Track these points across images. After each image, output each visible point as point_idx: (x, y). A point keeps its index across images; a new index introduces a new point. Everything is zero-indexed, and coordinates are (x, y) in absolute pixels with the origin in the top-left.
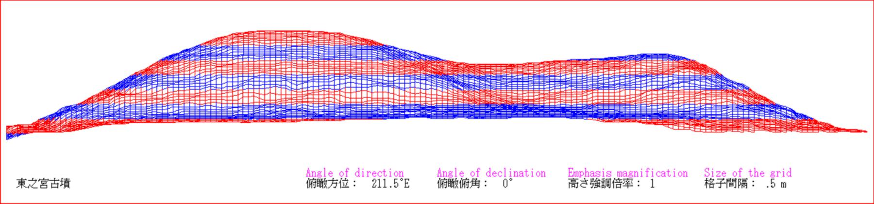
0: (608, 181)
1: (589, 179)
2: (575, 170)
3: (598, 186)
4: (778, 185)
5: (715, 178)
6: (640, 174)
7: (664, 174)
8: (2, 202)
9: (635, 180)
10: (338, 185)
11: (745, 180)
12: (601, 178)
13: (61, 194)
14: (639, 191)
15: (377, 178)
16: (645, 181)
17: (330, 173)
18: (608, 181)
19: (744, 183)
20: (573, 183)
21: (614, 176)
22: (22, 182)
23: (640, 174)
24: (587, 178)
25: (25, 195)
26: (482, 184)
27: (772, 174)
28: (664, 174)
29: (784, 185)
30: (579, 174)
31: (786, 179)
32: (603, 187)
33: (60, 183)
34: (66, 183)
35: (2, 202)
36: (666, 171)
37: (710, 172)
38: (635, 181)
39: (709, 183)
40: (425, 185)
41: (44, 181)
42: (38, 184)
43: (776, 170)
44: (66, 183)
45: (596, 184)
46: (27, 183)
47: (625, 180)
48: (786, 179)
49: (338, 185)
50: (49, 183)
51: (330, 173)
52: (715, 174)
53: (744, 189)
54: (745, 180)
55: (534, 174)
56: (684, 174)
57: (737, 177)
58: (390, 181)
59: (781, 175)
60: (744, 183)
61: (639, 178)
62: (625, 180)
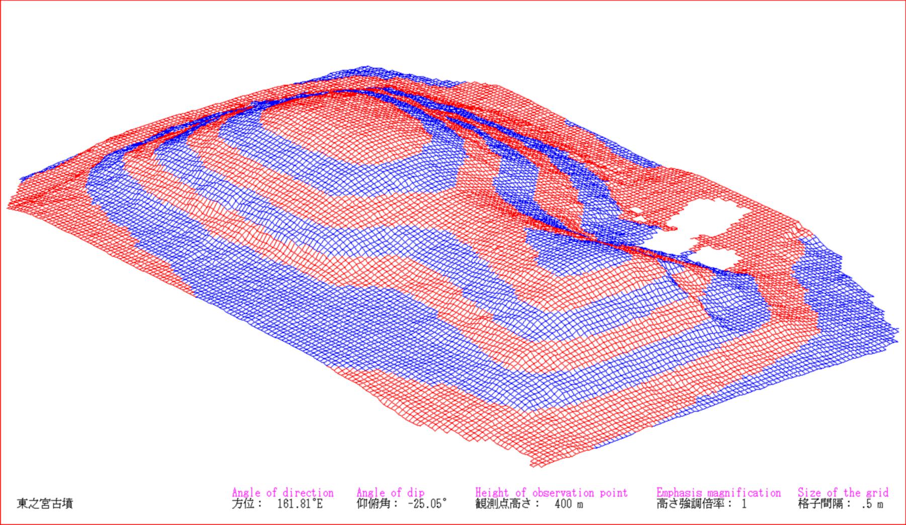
0: (699, 501)
1: (678, 499)
2: (664, 489)
3: (688, 506)
4: (875, 505)
5: (809, 498)
6: (731, 494)
7: (756, 494)
8: (2, 523)
9: (726, 500)
10: (243, 505)
11: (840, 500)
12: (691, 498)
13: (63, 514)
14: (731, 511)
15: (306, 498)
16: (737, 502)
17: (382, 493)
18: (699, 501)
19: (839, 504)
20: (662, 503)
21: (705, 496)
22: (22, 503)
23: (731, 494)
24: (676, 498)
25: (26, 515)
26: (392, 504)
27: (869, 493)
28: (756, 494)
29: (880, 505)
30: (669, 494)
31: (883, 499)
32: (693, 507)
33: (62, 503)
34: (69, 503)
35: (2, 523)
36: (758, 490)
37: (804, 491)
38: (726, 501)
39: (803, 503)
40: (344, 506)
41: (45, 502)
42: (40, 504)
43: (872, 489)
44: (69, 503)
45: (686, 504)
46: (28, 504)
47: (716, 500)
48: (883, 499)
49: (243, 505)
50: (51, 504)
51: (382, 493)
52: (809, 494)
53: (839, 509)
54: (840, 500)
55: (582, 494)
56: (777, 494)
57: (833, 497)
58: (297, 501)
59: (877, 495)
60: (839, 504)
61: (731, 498)
62: (716, 500)
